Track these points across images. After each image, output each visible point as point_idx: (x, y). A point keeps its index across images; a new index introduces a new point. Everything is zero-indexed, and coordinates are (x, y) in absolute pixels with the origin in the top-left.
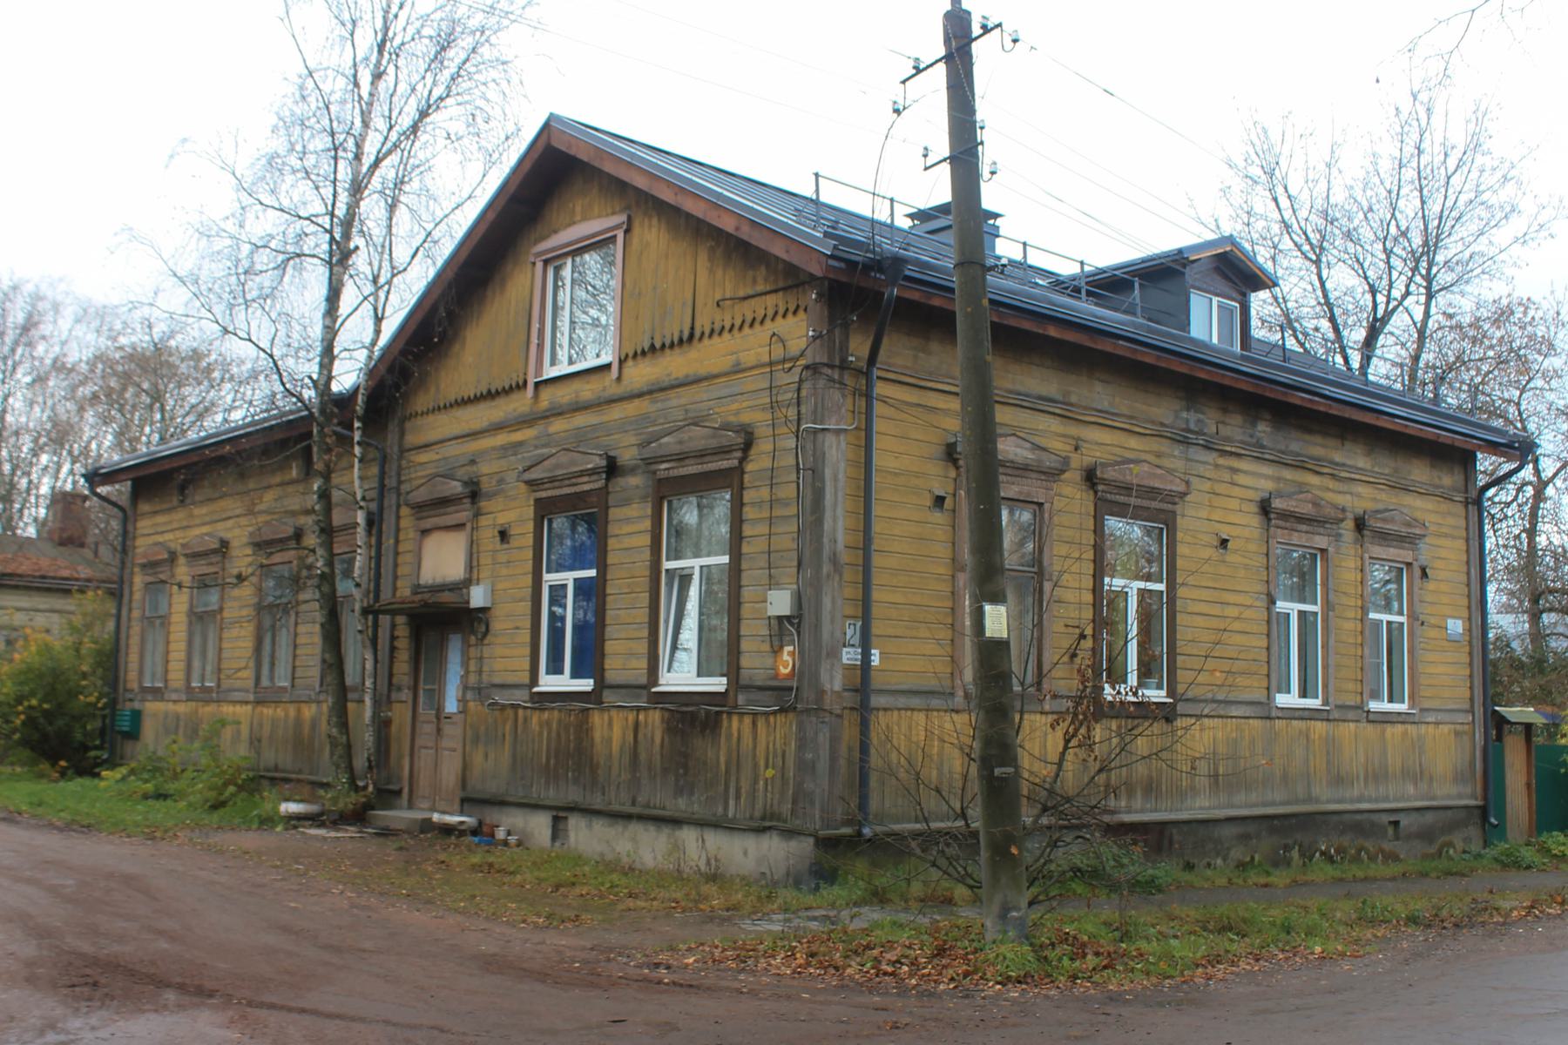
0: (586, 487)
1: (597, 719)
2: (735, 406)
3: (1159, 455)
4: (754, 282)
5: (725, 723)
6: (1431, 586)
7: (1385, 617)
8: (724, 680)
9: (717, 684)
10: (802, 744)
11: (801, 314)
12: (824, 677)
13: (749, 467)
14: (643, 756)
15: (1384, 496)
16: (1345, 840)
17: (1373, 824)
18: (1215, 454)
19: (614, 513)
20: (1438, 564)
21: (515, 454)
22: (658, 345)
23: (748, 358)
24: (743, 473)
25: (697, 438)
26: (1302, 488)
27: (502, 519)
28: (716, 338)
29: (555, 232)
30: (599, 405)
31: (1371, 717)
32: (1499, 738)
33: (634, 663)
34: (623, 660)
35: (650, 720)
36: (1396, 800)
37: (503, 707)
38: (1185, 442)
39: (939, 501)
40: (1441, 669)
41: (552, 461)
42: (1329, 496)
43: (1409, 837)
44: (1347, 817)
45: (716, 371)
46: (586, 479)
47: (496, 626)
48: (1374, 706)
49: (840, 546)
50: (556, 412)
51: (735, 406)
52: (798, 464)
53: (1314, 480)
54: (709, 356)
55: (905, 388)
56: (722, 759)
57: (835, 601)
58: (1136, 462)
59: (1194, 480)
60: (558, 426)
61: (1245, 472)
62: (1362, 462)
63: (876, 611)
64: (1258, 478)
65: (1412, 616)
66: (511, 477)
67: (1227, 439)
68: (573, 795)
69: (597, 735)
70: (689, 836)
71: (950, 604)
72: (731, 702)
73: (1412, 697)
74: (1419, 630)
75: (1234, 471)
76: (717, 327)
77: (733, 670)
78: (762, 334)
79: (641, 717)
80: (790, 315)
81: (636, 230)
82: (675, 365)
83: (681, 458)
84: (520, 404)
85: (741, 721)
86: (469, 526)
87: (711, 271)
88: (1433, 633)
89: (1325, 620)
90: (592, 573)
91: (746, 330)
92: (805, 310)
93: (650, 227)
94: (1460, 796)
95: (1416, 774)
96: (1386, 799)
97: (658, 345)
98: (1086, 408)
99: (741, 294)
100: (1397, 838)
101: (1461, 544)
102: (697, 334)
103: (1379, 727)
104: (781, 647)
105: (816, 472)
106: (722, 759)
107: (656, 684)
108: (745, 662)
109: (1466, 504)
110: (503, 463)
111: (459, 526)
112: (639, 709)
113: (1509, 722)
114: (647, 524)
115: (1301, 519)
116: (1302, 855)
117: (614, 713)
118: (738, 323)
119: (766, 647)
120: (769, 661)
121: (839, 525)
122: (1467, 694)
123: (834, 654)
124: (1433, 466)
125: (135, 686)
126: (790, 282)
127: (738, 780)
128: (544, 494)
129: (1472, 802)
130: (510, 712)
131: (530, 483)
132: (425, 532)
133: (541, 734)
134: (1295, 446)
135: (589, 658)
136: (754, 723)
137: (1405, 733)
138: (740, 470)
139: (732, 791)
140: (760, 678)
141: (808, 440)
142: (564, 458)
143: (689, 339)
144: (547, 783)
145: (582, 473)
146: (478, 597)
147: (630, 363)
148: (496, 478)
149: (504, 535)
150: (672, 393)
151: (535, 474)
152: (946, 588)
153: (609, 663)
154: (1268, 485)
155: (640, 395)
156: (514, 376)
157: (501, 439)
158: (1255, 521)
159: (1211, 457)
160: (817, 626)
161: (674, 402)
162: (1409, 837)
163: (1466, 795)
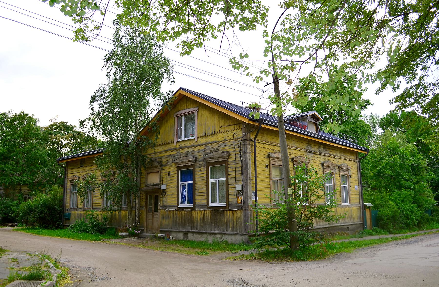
0: (190, 164)
1: (194, 213)
2: (226, 148)
3: (304, 155)
4: (229, 123)
5: (226, 213)
6: (352, 179)
7: (344, 186)
8: (225, 204)
9: (224, 205)
10: (244, 217)
11: (240, 129)
12: (249, 202)
13: (229, 160)
14: (206, 220)
15: (342, 161)
16: (339, 232)
17: (344, 228)
18: (314, 154)
19: (196, 169)
20: (353, 175)
21: (171, 157)
22: (207, 135)
23: (228, 138)
24: (228, 161)
25: (217, 154)
26: (329, 161)
27: (168, 170)
28: (220, 134)
29: (180, 111)
30: (192, 147)
31: (343, 206)
32: (365, 210)
33: (203, 201)
34: (200, 199)
35: (207, 212)
36: (348, 223)
37: (170, 211)
38: (308, 152)
39: (267, 166)
40: (354, 196)
41: (182, 158)
42: (333, 162)
43: (351, 230)
44: (339, 227)
45: (221, 140)
46: (190, 162)
47: (168, 193)
48: (343, 204)
49: (251, 176)
50: (181, 148)
51: (226, 148)
52: (241, 160)
53: (330, 159)
54: (219, 137)
55: (260, 144)
56: (225, 220)
57: (250, 187)
58: (301, 157)
59: (311, 160)
60: (182, 151)
61: (319, 158)
62: (339, 154)
63: (258, 189)
64: (321, 159)
65: (349, 185)
66: (170, 162)
67: (316, 151)
68: (189, 229)
69: (194, 216)
70: (218, 236)
71: (269, 187)
72: (227, 208)
73: (350, 202)
74: (350, 188)
75: (317, 157)
76: (221, 131)
77: (227, 202)
78: (232, 134)
79: (205, 212)
80: (238, 130)
81: (200, 111)
82: (211, 139)
83: (213, 158)
84: (173, 146)
85: (227, 212)
86: (160, 172)
87: (219, 120)
88: (352, 189)
89: (334, 187)
90: (192, 182)
91: (227, 132)
92: (241, 129)
93: (203, 111)
94: (359, 222)
95: (351, 218)
96: (346, 223)
97: (207, 135)
98: (291, 146)
99: (226, 125)
100: (348, 231)
101: (356, 171)
102: (216, 133)
103: (344, 208)
104: (239, 197)
105: (246, 161)
106: (225, 220)
107: (209, 205)
108: (230, 200)
109: (357, 162)
110: (168, 159)
111: (157, 172)
112: (204, 210)
113: (367, 206)
114: (205, 172)
115: (329, 167)
116: (332, 235)
117: (198, 211)
118: (226, 131)
119: (235, 197)
120: (236, 200)
121: (250, 172)
122: (359, 201)
123: (250, 198)
124: (351, 155)
125: (69, 208)
126: (238, 123)
127: (229, 224)
128: (179, 165)
129: (361, 223)
130: (172, 212)
131: (176, 163)
132: (148, 173)
133: (180, 216)
134: (327, 152)
135: (191, 200)
136: (233, 213)
137: (349, 209)
138: (227, 161)
139: (228, 226)
140: (234, 203)
141: (243, 156)
142: (184, 158)
143: (213, 134)
144: (182, 227)
145: (189, 161)
146: (163, 187)
147: (199, 138)
148: (167, 162)
149: (169, 174)
150: (210, 145)
151: (177, 161)
152: (269, 183)
153: (196, 201)
154: (323, 160)
155: (202, 145)
156: (171, 140)
157: (167, 154)
158: (321, 167)
159: (313, 155)
160: (247, 192)
161: (211, 147)
162: (351, 230)
163: (357, 221)
